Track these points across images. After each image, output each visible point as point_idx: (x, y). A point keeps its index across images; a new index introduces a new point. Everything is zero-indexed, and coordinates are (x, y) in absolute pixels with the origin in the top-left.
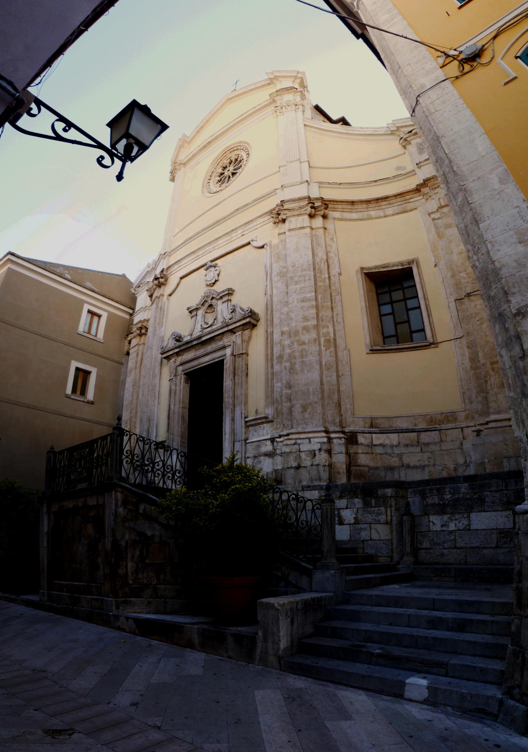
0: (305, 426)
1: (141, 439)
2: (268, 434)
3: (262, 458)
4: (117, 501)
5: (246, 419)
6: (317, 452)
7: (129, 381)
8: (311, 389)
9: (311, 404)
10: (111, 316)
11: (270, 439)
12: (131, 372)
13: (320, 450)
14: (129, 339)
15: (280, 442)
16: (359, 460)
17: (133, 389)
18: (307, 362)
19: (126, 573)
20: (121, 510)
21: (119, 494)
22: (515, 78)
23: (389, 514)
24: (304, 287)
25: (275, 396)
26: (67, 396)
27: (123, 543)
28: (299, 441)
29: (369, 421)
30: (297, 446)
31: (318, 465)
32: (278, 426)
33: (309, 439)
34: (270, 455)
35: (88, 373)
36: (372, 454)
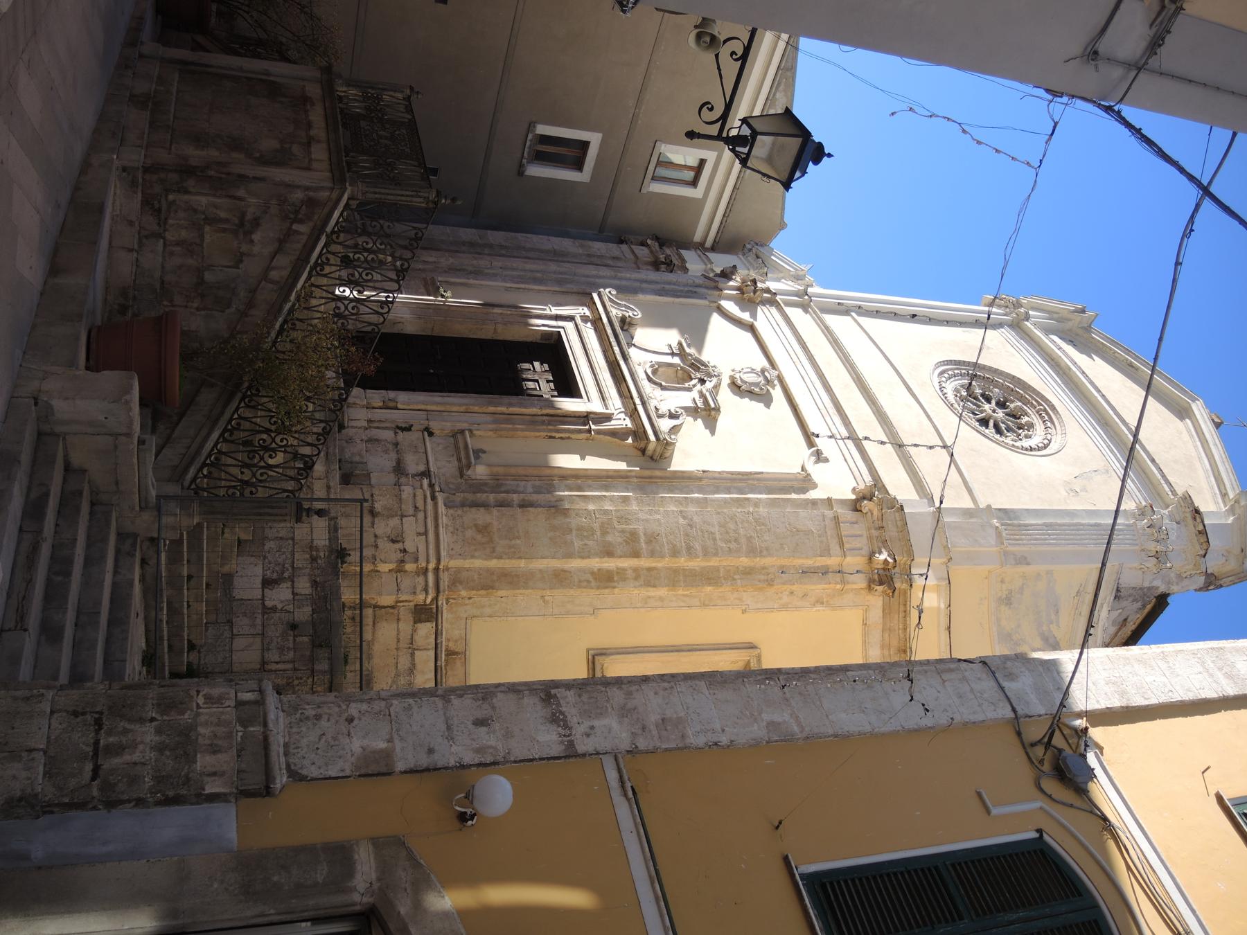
0: (451, 529)
3: (393, 455)
4: (316, 189)
5: (467, 433)
6: (400, 546)
7: (566, 244)
8: (518, 542)
9: (491, 541)
10: (699, 204)
12: (582, 246)
13: (405, 551)
14: (649, 242)
16: (385, 624)
18: (568, 537)
19: (187, 192)
20: (299, 195)
21: (327, 194)
22: (988, 812)
23: (281, 666)
24: (715, 539)
26: (531, 126)
27: (241, 193)
28: (421, 515)
29: (459, 648)
30: (411, 511)
31: (376, 546)
33: (426, 533)
34: (399, 469)
35: (578, 165)
36: (397, 649)
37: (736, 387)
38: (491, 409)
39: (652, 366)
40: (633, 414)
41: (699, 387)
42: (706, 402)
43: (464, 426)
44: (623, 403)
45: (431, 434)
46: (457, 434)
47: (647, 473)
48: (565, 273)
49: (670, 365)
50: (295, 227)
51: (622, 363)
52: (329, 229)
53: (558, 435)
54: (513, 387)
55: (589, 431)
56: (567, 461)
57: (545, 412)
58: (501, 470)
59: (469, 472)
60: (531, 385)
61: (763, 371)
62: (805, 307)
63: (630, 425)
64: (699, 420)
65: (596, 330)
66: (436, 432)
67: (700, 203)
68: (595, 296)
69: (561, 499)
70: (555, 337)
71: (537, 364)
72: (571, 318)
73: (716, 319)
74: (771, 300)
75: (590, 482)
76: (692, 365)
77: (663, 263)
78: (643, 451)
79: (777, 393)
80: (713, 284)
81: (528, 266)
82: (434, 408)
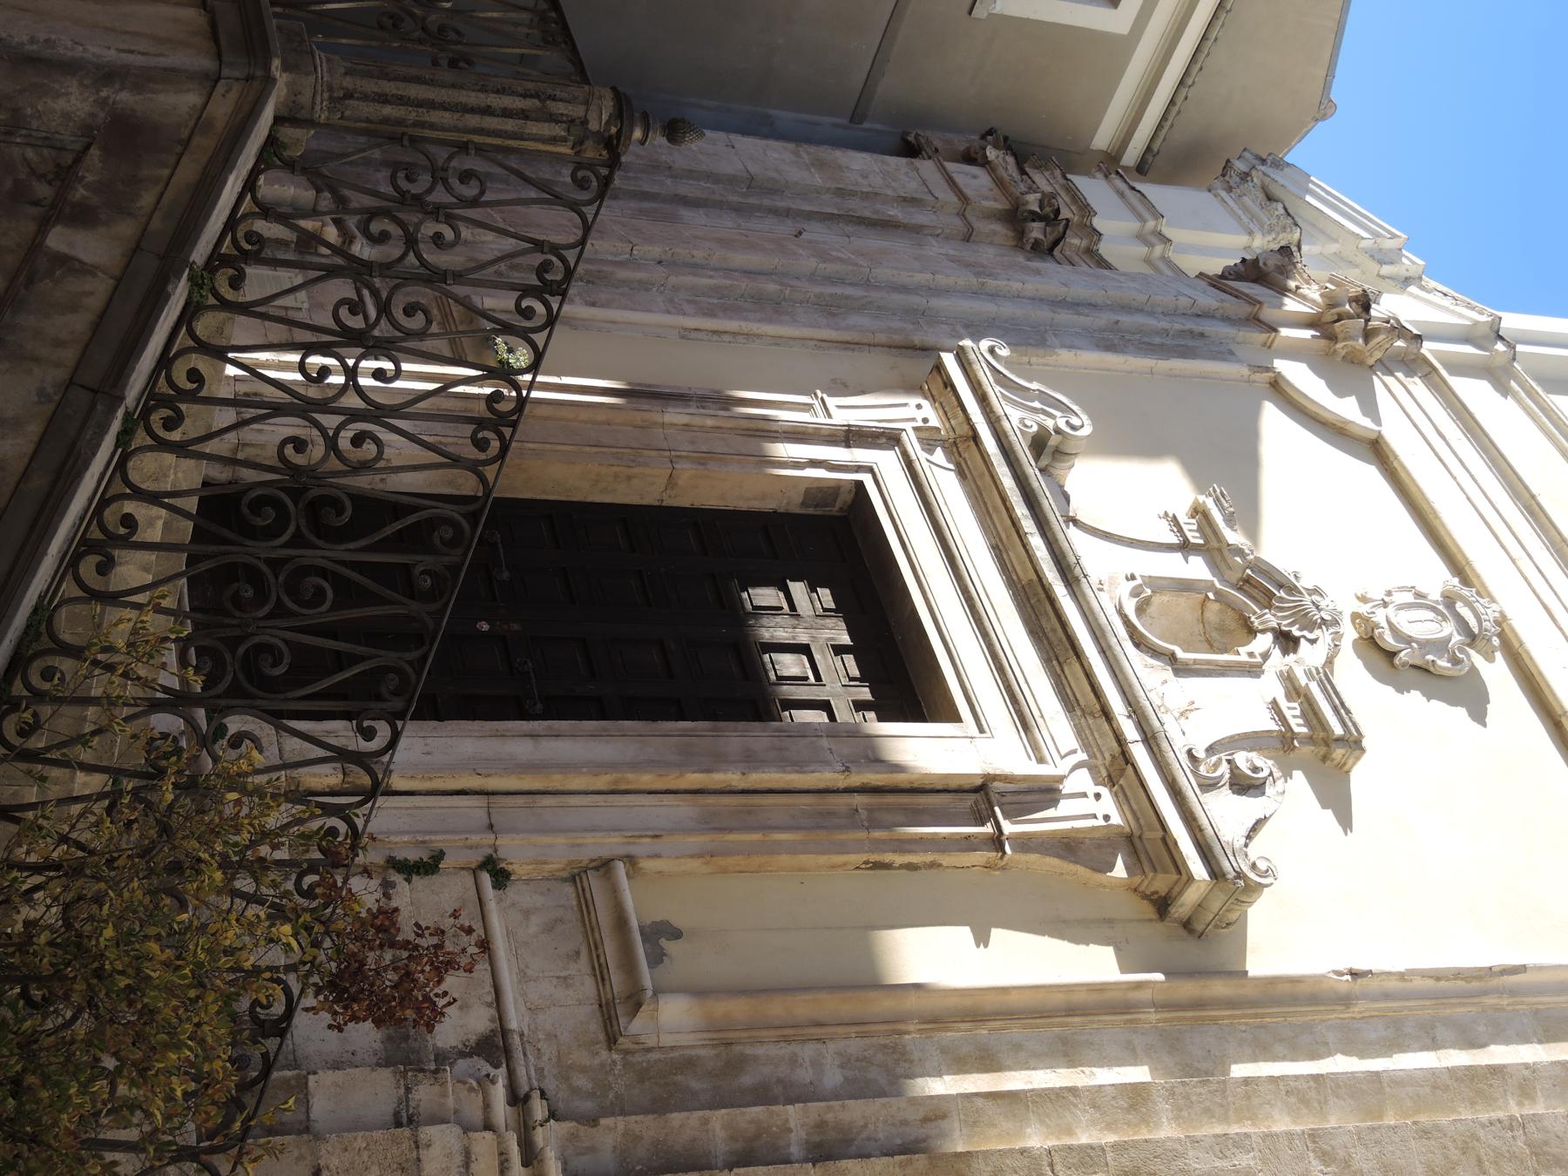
1: (556, 275)
2: (533, 1010)
4: (144, 79)
5: (621, 869)
10: (1118, 49)
11: (505, 1032)
12: (821, 165)
14: (991, 153)
15: (487, 1106)
17: (732, 181)
20: (74, 102)
25: (760, 1051)
32: (582, 1082)
37: (1381, 654)
38: (694, 779)
39: (1135, 593)
40: (1116, 771)
41: (1277, 661)
42: (1311, 712)
43: (609, 845)
44: (1079, 732)
45: (501, 878)
46: (587, 878)
47: (1188, 989)
48: (841, 281)
49: (1184, 586)
50: (57, 239)
51: (1060, 590)
52: (200, 254)
53: (899, 859)
54: (737, 690)
55: (997, 841)
56: (932, 956)
57: (856, 779)
58: (738, 1008)
59: (638, 1025)
60: (790, 664)
61: (1449, 600)
62: (1499, 376)
63: (1116, 819)
64: (1298, 775)
65: (962, 473)
66: (519, 869)
67: (1120, 48)
68: (949, 360)
69: (938, 1110)
70: (846, 497)
71: (798, 589)
72: (888, 438)
73: (1272, 419)
74: (1405, 353)
75: (1016, 1032)
76: (1245, 584)
77: (1035, 217)
78: (1162, 905)
79: (1496, 674)
80: (1244, 309)
81: (740, 259)
82: (512, 783)
